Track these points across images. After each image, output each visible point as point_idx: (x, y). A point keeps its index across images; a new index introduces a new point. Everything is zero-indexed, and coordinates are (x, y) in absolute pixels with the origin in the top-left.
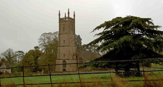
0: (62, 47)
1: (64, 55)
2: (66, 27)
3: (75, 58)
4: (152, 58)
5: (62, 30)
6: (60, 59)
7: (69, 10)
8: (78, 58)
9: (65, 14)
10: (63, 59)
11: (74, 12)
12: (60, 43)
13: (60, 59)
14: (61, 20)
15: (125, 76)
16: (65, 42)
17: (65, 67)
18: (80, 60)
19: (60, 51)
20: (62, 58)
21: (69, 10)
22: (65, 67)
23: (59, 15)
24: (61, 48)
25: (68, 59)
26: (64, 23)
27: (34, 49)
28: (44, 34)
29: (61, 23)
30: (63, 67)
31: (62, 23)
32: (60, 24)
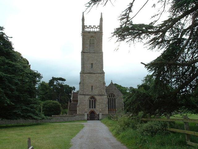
5: (88, 46)
7: (102, 15)
10: (90, 94)
17: (92, 108)
20: (87, 93)
21: (102, 15)
22: (92, 108)
30: (90, 108)
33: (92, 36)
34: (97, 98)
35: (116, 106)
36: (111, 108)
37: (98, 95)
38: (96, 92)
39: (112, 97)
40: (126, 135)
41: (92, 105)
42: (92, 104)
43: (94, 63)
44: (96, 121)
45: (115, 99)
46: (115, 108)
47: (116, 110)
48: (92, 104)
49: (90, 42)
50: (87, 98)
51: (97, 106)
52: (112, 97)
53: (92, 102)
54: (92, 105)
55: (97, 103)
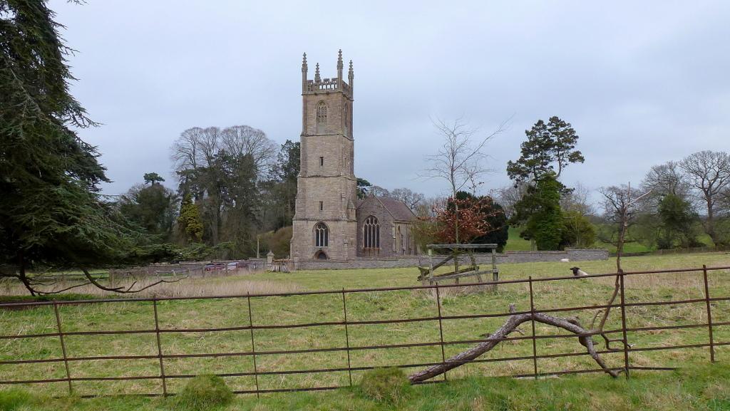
0: (314, 179)
1: (322, 205)
2: (328, 113)
3: (353, 217)
4: (484, 247)
5: (313, 121)
6: (307, 220)
7: (340, 55)
8: (364, 215)
9: (318, 69)
10: (318, 217)
11: (340, 52)
12: (306, 166)
13: (307, 220)
14: (311, 88)
15: (690, 247)
16: (324, 162)
17: (322, 245)
18: (368, 222)
19: (304, 190)
20: (312, 216)
21: (340, 55)
22: (322, 245)
23: (303, 69)
24: (307, 181)
25: (337, 220)
26: (322, 98)
27: (144, 181)
28: (193, 133)
29: (310, 98)
30: (317, 245)
31: (316, 97)
32: (305, 102)
33: (322, 102)
34: (330, 225)
35: (380, 242)
36: (370, 246)
37: (332, 220)
38: (327, 214)
39: (372, 223)
40: (452, 301)
41: (322, 241)
42: (322, 238)
43: (325, 156)
44: (680, 252)
45: (378, 227)
46: (378, 246)
47: (381, 249)
48: (322, 238)
49: (318, 113)
50: (312, 225)
51: (330, 242)
52: (372, 223)
53: (322, 234)
54: (322, 241)
55: (330, 236)
